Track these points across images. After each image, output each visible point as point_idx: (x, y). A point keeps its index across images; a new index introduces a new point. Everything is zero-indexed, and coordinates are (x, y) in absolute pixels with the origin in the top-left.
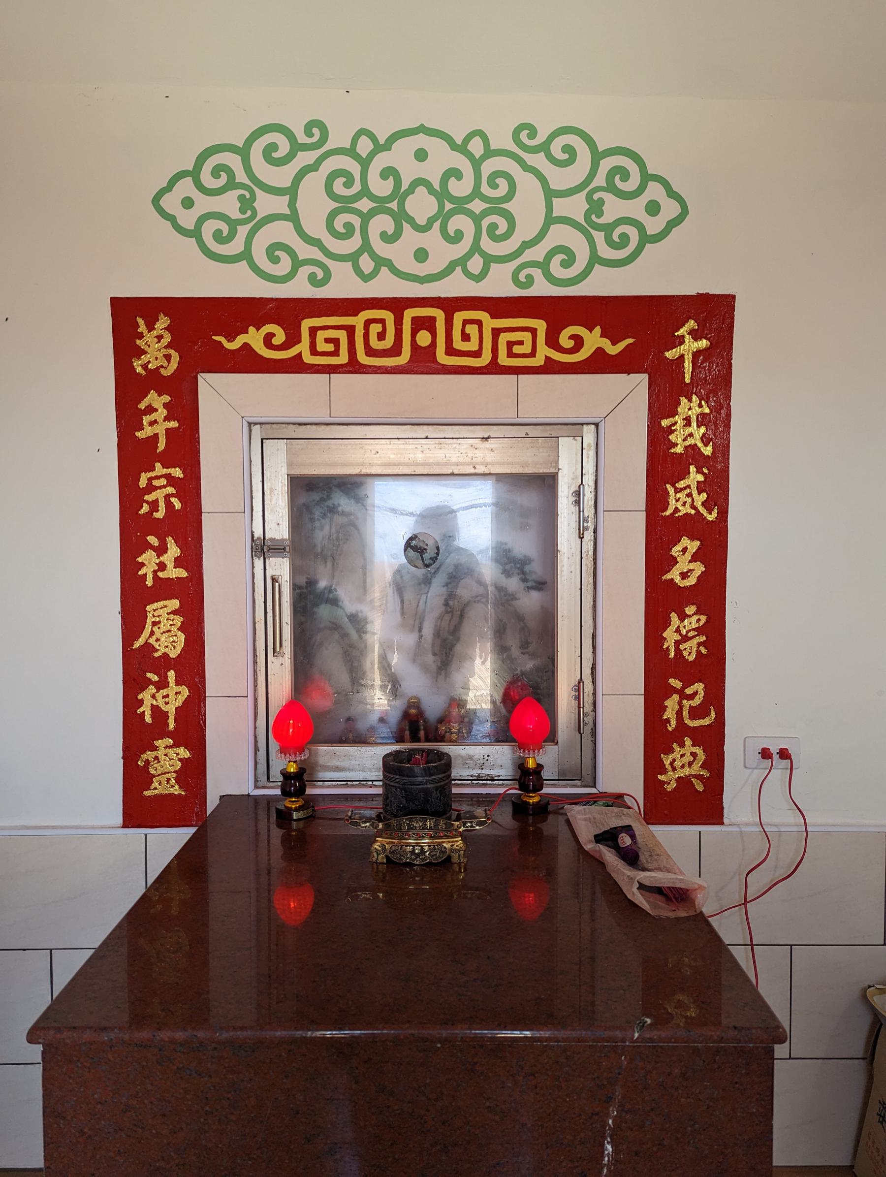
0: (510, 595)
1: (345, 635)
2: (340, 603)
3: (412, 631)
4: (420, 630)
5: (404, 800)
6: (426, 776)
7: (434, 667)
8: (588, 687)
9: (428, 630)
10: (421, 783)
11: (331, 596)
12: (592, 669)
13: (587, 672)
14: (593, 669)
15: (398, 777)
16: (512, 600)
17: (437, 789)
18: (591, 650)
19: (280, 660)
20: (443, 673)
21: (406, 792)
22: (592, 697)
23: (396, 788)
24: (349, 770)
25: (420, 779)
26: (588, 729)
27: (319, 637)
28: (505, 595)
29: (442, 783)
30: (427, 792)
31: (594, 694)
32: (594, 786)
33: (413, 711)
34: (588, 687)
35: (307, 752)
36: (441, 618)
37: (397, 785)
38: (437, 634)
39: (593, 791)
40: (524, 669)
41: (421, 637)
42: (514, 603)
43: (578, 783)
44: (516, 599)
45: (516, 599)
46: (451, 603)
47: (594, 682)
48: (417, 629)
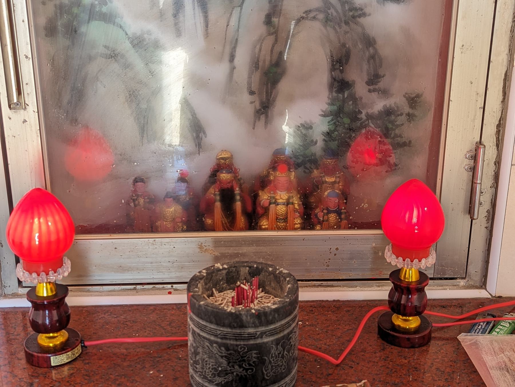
0: (356, 9)
1: (127, 66)
2: (118, 20)
3: (220, 59)
4: (232, 58)
5: (224, 362)
6: (261, 324)
7: (250, 110)
8: (489, 153)
9: (243, 58)
10: (252, 336)
11: (104, 9)
12: (498, 126)
13: (490, 130)
14: (501, 127)
15: (213, 326)
16: (360, 16)
17: (277, 342)
18: (501, 98)
19: (22, 114)
20: (263, 117)
21: (227, 349)
22: (492, 167)
23: (211, 342)
24: (138, 269)
25: (251, 330)
26: (481, 212)
27: (93, 68)
28: (351, 10)
29: (286, 332)
30: (261, 349)
31: (498, 163)
32: (483, 285)
33: (224, 176)
34: (489, 153)
35: (67, 264)
36: (261, 40)
37: (212, 338)
38: (255, 64)
39: (481, 294)
40: (370, 111)
41: (233, 69)
42: (362, 20)
43: (462, 283)
44: (364, 15)
45: (364, 15)
46: (275, 20)
47: (499, 144)
48: (227, 57)
